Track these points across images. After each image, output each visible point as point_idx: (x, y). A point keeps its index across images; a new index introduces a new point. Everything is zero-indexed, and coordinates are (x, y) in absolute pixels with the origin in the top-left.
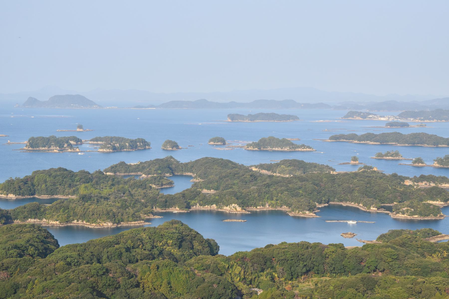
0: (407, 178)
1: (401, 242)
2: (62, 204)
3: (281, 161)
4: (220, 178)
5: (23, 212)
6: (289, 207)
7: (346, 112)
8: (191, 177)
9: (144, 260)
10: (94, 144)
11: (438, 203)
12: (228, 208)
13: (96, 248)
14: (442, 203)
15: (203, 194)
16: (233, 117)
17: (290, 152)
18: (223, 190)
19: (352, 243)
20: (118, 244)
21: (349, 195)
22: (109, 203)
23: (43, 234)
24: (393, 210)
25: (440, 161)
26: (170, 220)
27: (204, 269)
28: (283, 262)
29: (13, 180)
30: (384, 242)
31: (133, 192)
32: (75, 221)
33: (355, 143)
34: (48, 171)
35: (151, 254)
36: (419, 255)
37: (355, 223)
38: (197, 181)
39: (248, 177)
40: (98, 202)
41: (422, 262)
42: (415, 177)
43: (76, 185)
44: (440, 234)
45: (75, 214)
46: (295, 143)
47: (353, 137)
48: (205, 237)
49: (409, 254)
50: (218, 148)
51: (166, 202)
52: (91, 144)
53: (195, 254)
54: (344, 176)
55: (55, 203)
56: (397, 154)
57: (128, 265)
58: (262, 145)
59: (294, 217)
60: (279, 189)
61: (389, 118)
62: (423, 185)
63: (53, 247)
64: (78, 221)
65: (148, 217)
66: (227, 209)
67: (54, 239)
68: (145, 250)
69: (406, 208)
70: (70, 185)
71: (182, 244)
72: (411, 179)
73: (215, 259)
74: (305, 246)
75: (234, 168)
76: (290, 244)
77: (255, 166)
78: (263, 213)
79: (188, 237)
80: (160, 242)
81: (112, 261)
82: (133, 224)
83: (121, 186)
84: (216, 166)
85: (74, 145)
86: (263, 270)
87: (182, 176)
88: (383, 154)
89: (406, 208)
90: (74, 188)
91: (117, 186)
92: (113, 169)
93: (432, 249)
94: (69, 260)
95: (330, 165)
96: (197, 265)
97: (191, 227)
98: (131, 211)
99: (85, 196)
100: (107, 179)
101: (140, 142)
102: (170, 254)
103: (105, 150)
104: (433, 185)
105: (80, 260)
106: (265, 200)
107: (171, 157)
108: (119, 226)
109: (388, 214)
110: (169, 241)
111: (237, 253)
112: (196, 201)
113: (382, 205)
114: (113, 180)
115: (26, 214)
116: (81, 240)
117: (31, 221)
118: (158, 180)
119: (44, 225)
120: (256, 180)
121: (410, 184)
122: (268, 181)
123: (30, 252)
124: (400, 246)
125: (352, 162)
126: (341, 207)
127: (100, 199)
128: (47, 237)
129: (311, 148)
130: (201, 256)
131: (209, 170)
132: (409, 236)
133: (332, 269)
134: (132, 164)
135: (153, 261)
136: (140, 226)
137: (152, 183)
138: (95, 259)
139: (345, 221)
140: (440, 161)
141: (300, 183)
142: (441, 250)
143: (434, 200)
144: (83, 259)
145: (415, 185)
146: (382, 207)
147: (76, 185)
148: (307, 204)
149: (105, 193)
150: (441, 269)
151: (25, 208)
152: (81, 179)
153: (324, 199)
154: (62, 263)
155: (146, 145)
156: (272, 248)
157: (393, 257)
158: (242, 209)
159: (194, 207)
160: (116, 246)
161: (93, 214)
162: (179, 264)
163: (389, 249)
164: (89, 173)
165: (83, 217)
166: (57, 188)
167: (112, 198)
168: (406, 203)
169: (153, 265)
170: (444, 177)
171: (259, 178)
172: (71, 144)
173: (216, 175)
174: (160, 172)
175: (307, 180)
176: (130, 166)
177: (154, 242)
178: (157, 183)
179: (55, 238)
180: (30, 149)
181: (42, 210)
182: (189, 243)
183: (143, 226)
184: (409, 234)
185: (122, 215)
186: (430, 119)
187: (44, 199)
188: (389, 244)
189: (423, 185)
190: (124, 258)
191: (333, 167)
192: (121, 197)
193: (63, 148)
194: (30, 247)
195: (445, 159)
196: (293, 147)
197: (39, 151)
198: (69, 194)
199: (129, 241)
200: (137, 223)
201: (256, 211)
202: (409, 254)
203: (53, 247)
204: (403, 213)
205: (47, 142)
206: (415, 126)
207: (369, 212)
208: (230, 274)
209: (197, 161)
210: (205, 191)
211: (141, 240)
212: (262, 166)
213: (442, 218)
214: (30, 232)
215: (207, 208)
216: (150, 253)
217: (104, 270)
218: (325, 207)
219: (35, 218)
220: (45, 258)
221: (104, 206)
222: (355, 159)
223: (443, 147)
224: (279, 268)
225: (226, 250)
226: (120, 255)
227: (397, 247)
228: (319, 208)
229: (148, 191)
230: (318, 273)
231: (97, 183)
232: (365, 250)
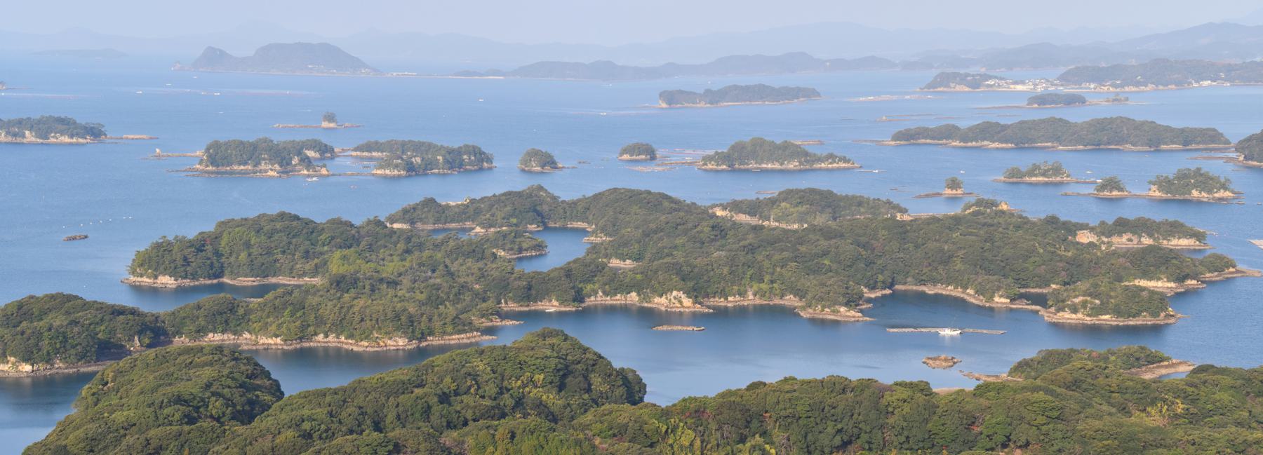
0: (1084, 227)
1: (1069, 378)
2: (287, 298)
3: (780, 194)
4: (646, 235)
5: (194, 319)
6: (801, 298)
7: (932, 74)
8: (583, 232)
9: (481, 422)
10: (362, 158)
11: (1162, 285)
12: (663, 300)
13: (370, 397)
14: (1172, 285)
15: (611, 269)
16: (671, 97)
17: (800, 171)
18: (651, 261)
19: (950, 381)
20: (421, 385)
21: (940, 268)
22: (400, 294)
23: (243, 368)
24: (1050, 303)
25: (1165, 184)
26: (538, 328)
27: (614, 435)
28: (788, 421)
29: (169, 243)
30: (1026, 378)
31: (453, 268)
32: (321, 337)
33: (954, 147)
34: (253, 220)
35: (498, 406)
36: (1114, 410)
37: (957, 333)
38: (598, 240)
39: (707, 229)
40: (373, 291)
41: (1121, 425)
42: (1103, 223)
43: (322, 254)
44: (1168, 359)
45: (320, 322)
46: (810, 150)
47: (949, 132)
48: (617, 365)
49: (1090, 406)
50: (639, 168)
51: (530, 289)
52: (356, 157)
53: (595, 401)
54: (929, 224)
55: (270, 296)
56: (1057, 170)
57: (445, 434)
58: (736, 159)
59: (813, 321)
60: (777, 257)
61: (1035, 85)
62: (1122, 241)
63: (268, 398)
64: (327, 336)
65: (490, 324)
66: (660, 302)
67: (270, 379)
68: (483, 397)
69: (1081, 298)
70: (307, 252)
71: (567, 380)
72: (1092, 229)
73: (638, 412)
74: (839, 386)
75: (675, 210)
76: (803, 382)
77: (721, 205)
78: (741, 312)
79: (579, 366)
80: (518, 379)
81: (409, 426)
82: (454, 339)
83: (426, 253)
84: (635, 208)
85: (316, 159)
86: (743, 440)
87: (564, 229)
88: (1024, 170)
89: (1081, 298)
90: (316, 261)
91: (417, 253)
92: (408, 214)
93: (1148, 396)
94: (306, 426)
95: (895, 201)
96: (599, 425)
97: (585, 342)
98: (450, 310)
99: (344, 277)
100: (395, 238)
101: (469, 153)
102: (540, 406)
103: (388, 172)
104: (1147, 241)
105: (334, 426)
106: (746, 281)
107: (541, 188)
108: (424, 344)
109: (1037, 312)
110: (536, 377)
111: (684, 400)
112: (597, 285)
113: (1023, 291)
114: (409, 239)
115: (202, 321)
116: (336, 380)
117: (215, 338)
118: (512, 239)
119: (246, 348)
120: (724, 237)
121: (1091, 240)
122: (751, 238)
123: (214, 412)
124: (1068, 388)
125: (948, 191)
126: (923, 295)
127: (377, 284)
128: (253, 374)
129: (848, 161)
130: (607, 406)
131: (621, 217)
132: (1090, 364)
133: (903, 439)
134: (452, 203)
135: (502, 421)
136: (471, 344)
137: (497, 247)
138: (368, 422)
139: (933, 330)
140: (1165, 184)
141: (824, 243)
142: (1169, 397)
143: (1151, 279)
144: (340, 422)
145: (1103, 243)
146: (1022, 296)
147: (322, 254)
148: (843, 291)
149: (390, 270)
150: (1169, 441)
151: (199, 308)
152: (333, 238)
153: (880, 278)
154: (290, 434)
155: (482, 161)
156: (761, 391)
157: (1049, 414)
158: (694, 303)
159: (593, 298)
160: (416, 390)
161: (362, 320)
162: (559, 426)
163: (1040, 396)
164: (352, 225)
165: (339, 326)
166: (276, 261)
167: (406, 281)
168: (1083, 285)
169: (501, 430)
170: (1176, 222)
171: (731, 233)
172: (308, 158)
173: (637, 228)
174: (514, 221)
175: (842, 236)
176: (448, 207)
177: (503, 380)
178: (509, 246)
179: (273, 376)
180: (210, 168)
181: (241, 311)
182: (581, 378)
183: (477, 344)
184: (1089, 358)
185: (430, 320)
186: (1137, 84)
187: (244, 287)
188: (1038, 382)
189: (1122, 241)
190: (435, 419)
191: (903, 205)
192: (426, 279)
193: (289, 168)
194: (213, 399)
195: (1178, 178)
196: (807, 161)
197: (232, 173)
198: (304, 274)
199: (448, 380)
200: (463, 338)
201: (726, 308)
202: (1090, 406)
203: (268, 398)
204: (1074, 310)
205: (252, 152)
206: (1100, 101)
207: (991, 309)
208: (671, 446)
209: (597, 197)
210: (615, 263)
211: (474, 376)
212: (736, 206)
213: (1172, 321)
214: (211, 365)
215: (619, 299)
216: (494, 403)
217: (391, 447)
218: (884, 296)
219: (223, 332)
220: (250, 423)
221: (386, 301)
222: (954, 184)
223: (1172, 151)
224: (779, 435)
225: (664, 390)
226: (427, 410)
227: (1059, 390)
228: (869, 300)
229: (489, 265)
230: (870, 449)
231: (370, 248)
232: (981, 396)
